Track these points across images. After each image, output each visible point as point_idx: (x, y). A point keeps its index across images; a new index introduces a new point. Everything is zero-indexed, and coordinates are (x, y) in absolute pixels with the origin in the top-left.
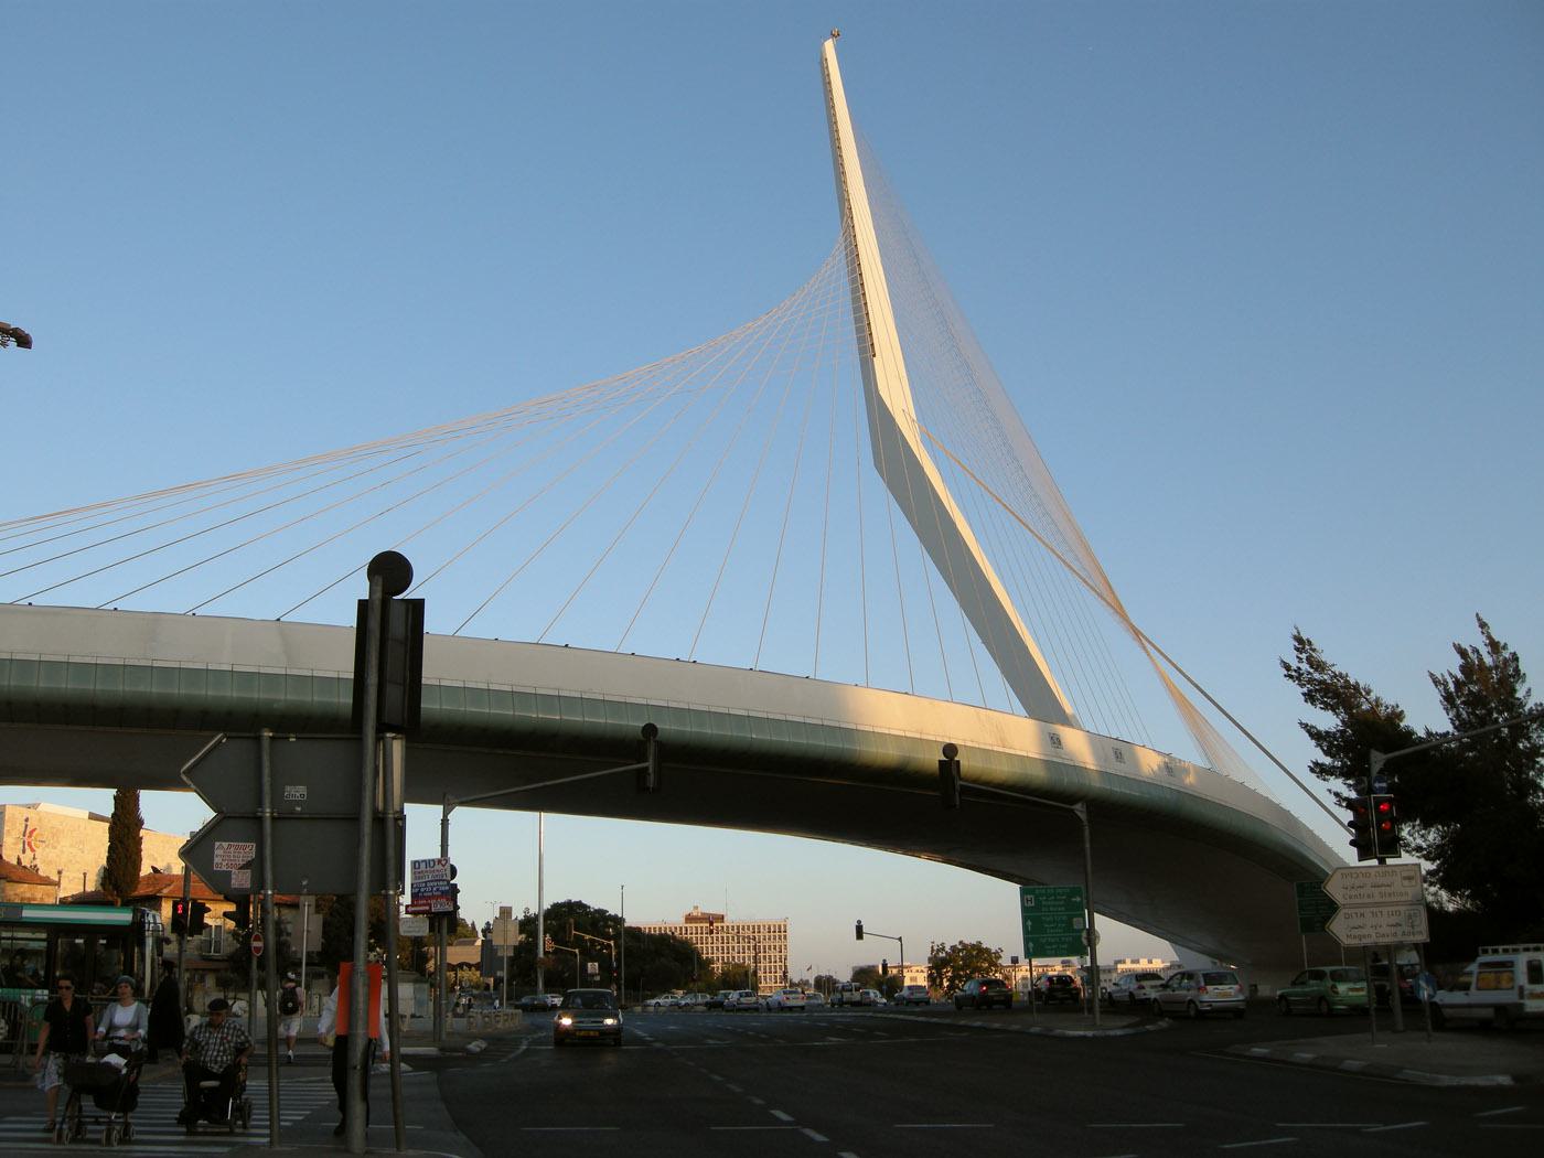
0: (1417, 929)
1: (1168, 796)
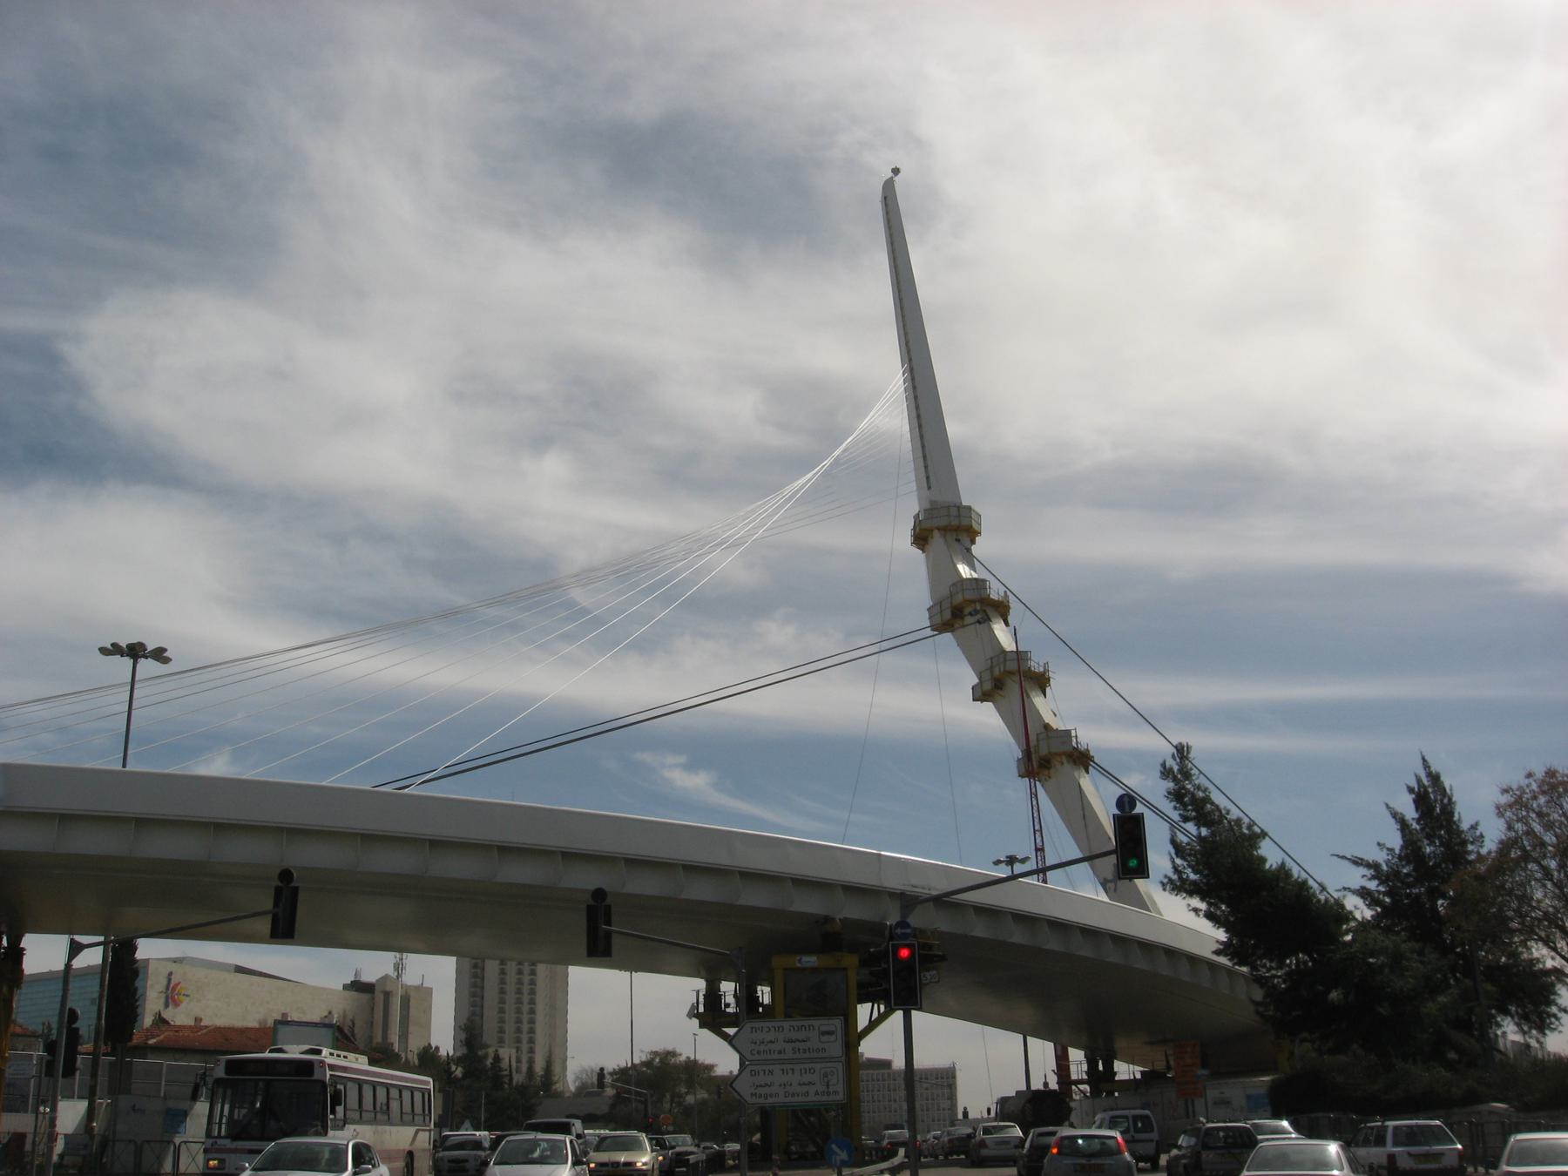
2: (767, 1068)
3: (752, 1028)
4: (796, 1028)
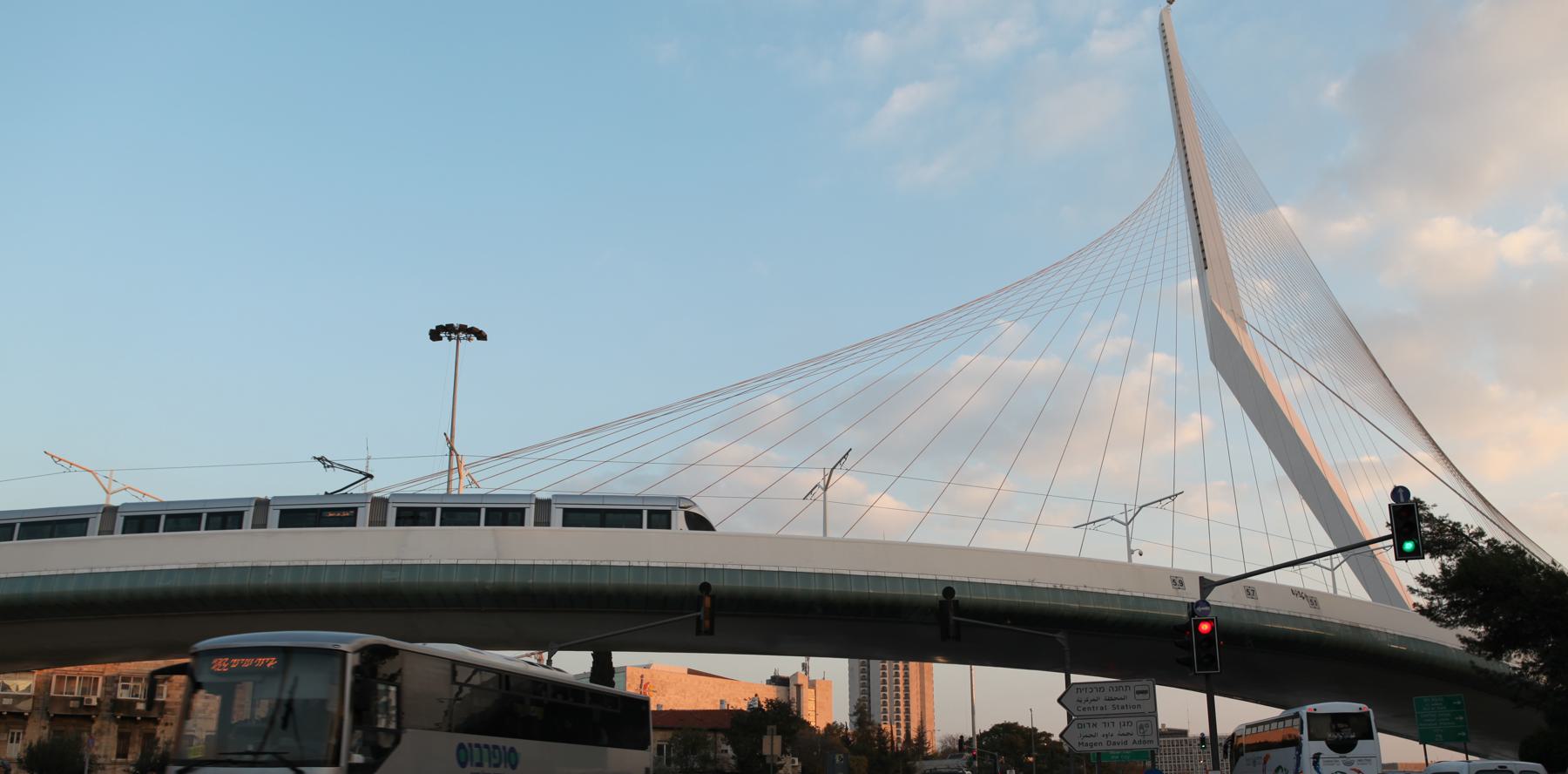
0: (1147, 738)
1: (1414, 650)
2: (1091, 721)
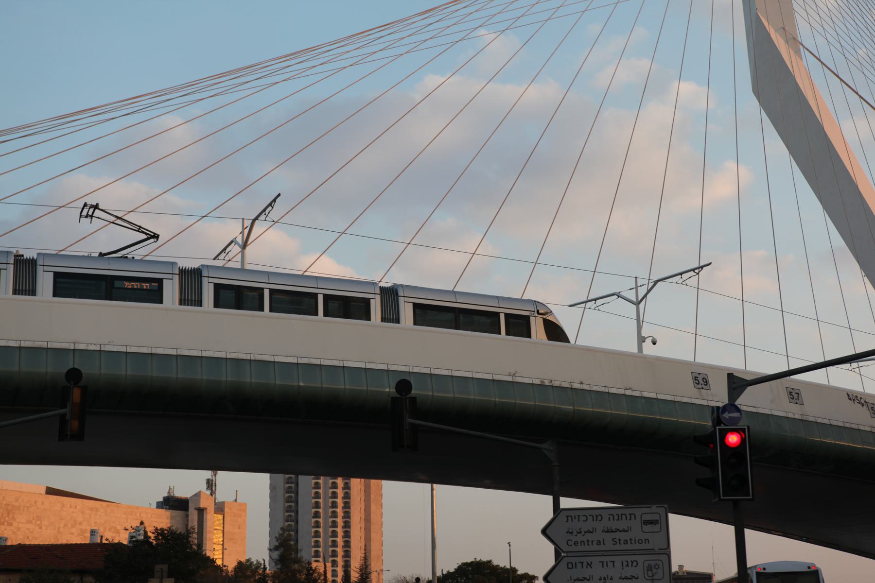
2: (585, 560)
3: (567, 517)
4: (616, 517)
